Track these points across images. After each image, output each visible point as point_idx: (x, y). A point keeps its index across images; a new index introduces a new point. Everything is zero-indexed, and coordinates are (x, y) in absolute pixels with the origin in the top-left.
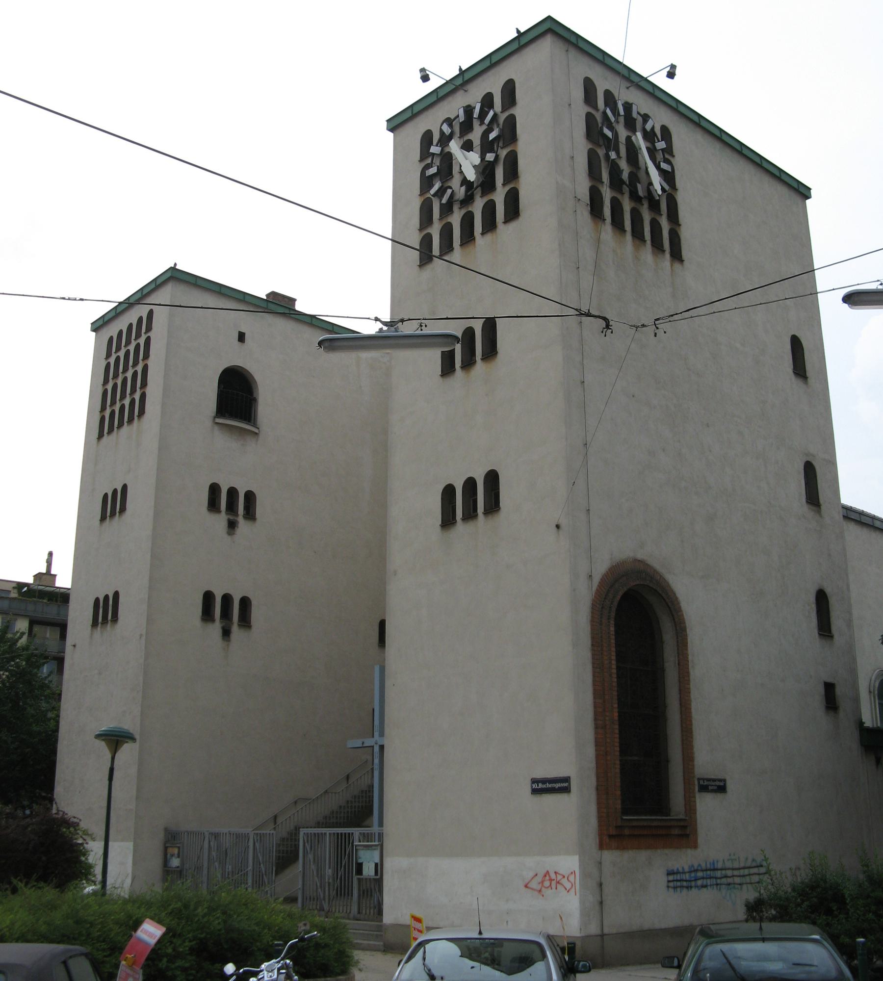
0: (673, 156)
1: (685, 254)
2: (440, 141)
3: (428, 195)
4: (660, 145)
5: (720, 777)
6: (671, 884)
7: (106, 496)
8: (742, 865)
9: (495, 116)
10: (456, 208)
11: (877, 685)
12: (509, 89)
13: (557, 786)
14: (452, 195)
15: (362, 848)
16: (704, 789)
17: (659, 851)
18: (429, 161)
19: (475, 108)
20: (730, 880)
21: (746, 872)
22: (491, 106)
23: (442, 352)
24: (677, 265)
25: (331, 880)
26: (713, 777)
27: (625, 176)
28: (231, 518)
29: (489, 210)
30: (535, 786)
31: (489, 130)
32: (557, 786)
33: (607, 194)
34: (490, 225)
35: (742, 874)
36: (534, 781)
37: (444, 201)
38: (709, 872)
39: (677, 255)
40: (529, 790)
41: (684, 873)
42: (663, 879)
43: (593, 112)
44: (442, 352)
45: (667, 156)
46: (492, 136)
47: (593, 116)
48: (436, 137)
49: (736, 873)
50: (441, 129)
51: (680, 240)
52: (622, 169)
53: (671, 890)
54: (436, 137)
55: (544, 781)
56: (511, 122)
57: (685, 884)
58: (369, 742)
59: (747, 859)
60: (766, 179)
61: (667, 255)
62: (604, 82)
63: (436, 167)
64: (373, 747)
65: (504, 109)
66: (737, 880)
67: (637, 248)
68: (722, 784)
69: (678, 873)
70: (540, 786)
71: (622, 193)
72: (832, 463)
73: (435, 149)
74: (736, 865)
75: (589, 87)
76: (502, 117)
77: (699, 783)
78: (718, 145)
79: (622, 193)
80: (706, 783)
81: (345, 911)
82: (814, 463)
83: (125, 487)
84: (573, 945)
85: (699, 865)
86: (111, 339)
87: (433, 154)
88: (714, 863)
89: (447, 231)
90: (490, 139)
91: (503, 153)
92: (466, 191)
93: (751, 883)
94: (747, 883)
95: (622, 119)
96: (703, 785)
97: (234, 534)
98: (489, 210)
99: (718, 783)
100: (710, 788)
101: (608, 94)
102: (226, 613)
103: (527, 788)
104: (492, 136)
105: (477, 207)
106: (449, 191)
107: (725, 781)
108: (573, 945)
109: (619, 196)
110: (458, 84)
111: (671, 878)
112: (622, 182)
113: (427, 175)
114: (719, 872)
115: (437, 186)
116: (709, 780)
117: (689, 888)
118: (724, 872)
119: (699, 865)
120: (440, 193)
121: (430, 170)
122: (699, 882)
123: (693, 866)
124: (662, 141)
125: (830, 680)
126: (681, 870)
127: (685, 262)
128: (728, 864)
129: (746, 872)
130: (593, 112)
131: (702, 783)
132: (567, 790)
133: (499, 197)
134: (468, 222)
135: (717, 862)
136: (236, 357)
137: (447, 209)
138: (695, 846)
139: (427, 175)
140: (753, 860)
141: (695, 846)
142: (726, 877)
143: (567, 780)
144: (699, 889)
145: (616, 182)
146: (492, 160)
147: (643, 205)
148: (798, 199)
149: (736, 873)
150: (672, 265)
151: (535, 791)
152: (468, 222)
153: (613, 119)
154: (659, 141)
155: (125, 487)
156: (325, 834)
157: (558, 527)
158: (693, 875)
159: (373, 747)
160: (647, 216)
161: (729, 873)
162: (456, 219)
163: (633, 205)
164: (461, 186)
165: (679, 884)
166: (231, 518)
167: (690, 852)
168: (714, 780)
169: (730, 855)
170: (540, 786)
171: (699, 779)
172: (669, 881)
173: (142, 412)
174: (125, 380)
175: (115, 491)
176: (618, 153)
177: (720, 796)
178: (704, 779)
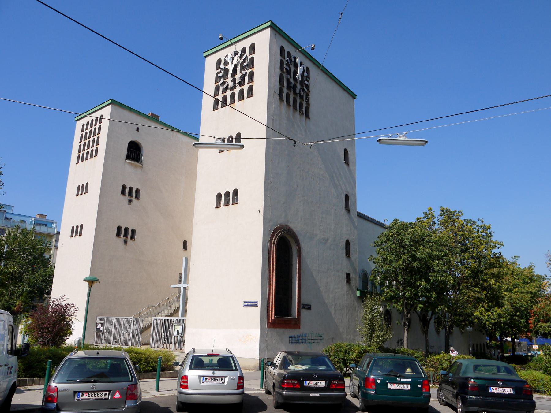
0: (310, 79)
1: (311, 116)
2: (224, 63)
3: (218, 84)
4: (306, 74)
5: (309, 304)
6: (291, 341)
7: (79, 187)
8: (315, 336)
9: (247, 56)
10: (228, 90)
11: (362, 275)
12: (253, 47)
13: (253, 304)
14: (228, 85)
15: (177, 325)
16: (303, 308)
17: (287, 329)
18: (219, 70)
19: (239, 52)
20: (310, 341)
21: (316, 338)
22: (245, 52)
23: (240, 143)
24: (307, 120)
25: (164, 337)
26: (306, 304)
27: (292, 85)
28: (130, 198)
29: (242, 92)
30: (245, 304)
31: (244, 62)
32: (253, 304)
33: (285, 91)
34: (241, 98)
35: (314, 339)
36: (245, 302)
37: (224, 87)
38: (303, 338)
39: (308, 116)
40: (243, 305)
41: (295, 337)
42: (288, 339)
43: (283, 59)
44: (240, 143)
45: (308, 79)
46: (245, 64)
47: (283, 60)
48: (223, 62)
49: (313, 338)
50: (225, 59)
51: (309, 110)
52: (291, 82)
53: (290, 343)
54: (223, 62)
55: (248, 302)
56: (252, 60)
57: (295, 341)
58: (179, 286)
59: (316, 334)
60: (341, 90)
61: (304, 116)
62: (288, 48)
63: (222, 74)
64: (181, 287)
65: (250, 54)
66: (313, 341)
67: (294, 112)
68: (310, 307)
69: (293, 337)
70: (247, 304)
71: (291, 91)
72: (355, 195)
73: (222, 66)
74: (313, 336)
75: (282, 49)
76: (249, 57)
77: (302, 306)
78: (325, 76)
79: (291, 91)
80: (304, 306)
81: (168, 348)
82: (349, 195)
83: (87, 184)
84: (234, 368)
85: (300, 335)
86: (84, 125)
87: (221, 68)
88: (305, 335)
89: (225, 98)
90: (244, 65)
91: (249, 71)
92: (233, 84)
93: (317, 342)
94: (316, 342)
95: (293, 63)
96: (303, 307)
97: (131, 205)
98: (242, 92)
99: (308, 306)
100: (306, 308)
101: (289, 54)
102: (126, 235)
103: (243, 304)
104: (245, 64)
105: (237, 90)
106: (226, 84)
107: (311, 305)
108: (234, 368)
109: (289, 92)
110: (233, 42)
111: (291, 339)
112: (291, 87)
113: (218, 76)
114: (307, 338)
115: (222, 80)
116: (305, 305)
117: (296, 343)
118: (308, 338)
119: (300, 335)
120: (223, 83)
121: (220, 74)
122: (300, 341)
123: (298, 335)
124: (306, 73)
125: (349, 272)
126: (294, 336)
127: (310, 119)
128: (310, 335)
129: (316, 338)
130: (283, 59)
131: (303, 306)
132: (256, 306)
133: (246, 87)
134: (233, 96)
135: (307, 334)
136: (136, 137)
137: (225, 90)
138: (299, 328)
139: (218, 76)
140: (319, 334)
141: (299, 328)
142: (309, 340)
143: (257, 302)
144: (300, 343)
145: (289, 87)
146: (244, 73)
147: (297, 96)
148: (351, 98)
149: (313, 338)
150: (306, 120)
151: (245, 306)
152: (233, 96)
153: (290, 63)
154: (305, 73)
155: (87, 184)
156: (163, 319)
157: (259, 211)
158: (298, 338)
159: (181, 287)
160: (298, 101)
161: (310, 338)
162: (228, 94)
163: (294, 96)
164: (231, 82)
165: (293, 341)
166: (130, 198)
167: (297, 330)
168: (307, 305)
169: (311, 332)
170: (247, 304)
171: (302, 304)
172: (290, 340)
173: (96, 155)
174: (89, 142)
175: (83, 185)
176: (290, 76)
177: (309, 311)
178: (304, 304)
